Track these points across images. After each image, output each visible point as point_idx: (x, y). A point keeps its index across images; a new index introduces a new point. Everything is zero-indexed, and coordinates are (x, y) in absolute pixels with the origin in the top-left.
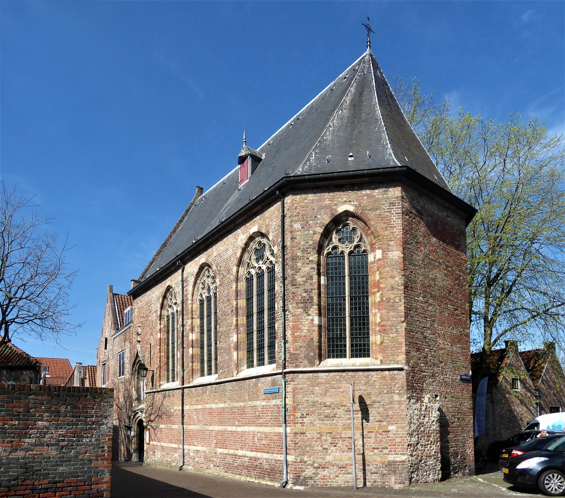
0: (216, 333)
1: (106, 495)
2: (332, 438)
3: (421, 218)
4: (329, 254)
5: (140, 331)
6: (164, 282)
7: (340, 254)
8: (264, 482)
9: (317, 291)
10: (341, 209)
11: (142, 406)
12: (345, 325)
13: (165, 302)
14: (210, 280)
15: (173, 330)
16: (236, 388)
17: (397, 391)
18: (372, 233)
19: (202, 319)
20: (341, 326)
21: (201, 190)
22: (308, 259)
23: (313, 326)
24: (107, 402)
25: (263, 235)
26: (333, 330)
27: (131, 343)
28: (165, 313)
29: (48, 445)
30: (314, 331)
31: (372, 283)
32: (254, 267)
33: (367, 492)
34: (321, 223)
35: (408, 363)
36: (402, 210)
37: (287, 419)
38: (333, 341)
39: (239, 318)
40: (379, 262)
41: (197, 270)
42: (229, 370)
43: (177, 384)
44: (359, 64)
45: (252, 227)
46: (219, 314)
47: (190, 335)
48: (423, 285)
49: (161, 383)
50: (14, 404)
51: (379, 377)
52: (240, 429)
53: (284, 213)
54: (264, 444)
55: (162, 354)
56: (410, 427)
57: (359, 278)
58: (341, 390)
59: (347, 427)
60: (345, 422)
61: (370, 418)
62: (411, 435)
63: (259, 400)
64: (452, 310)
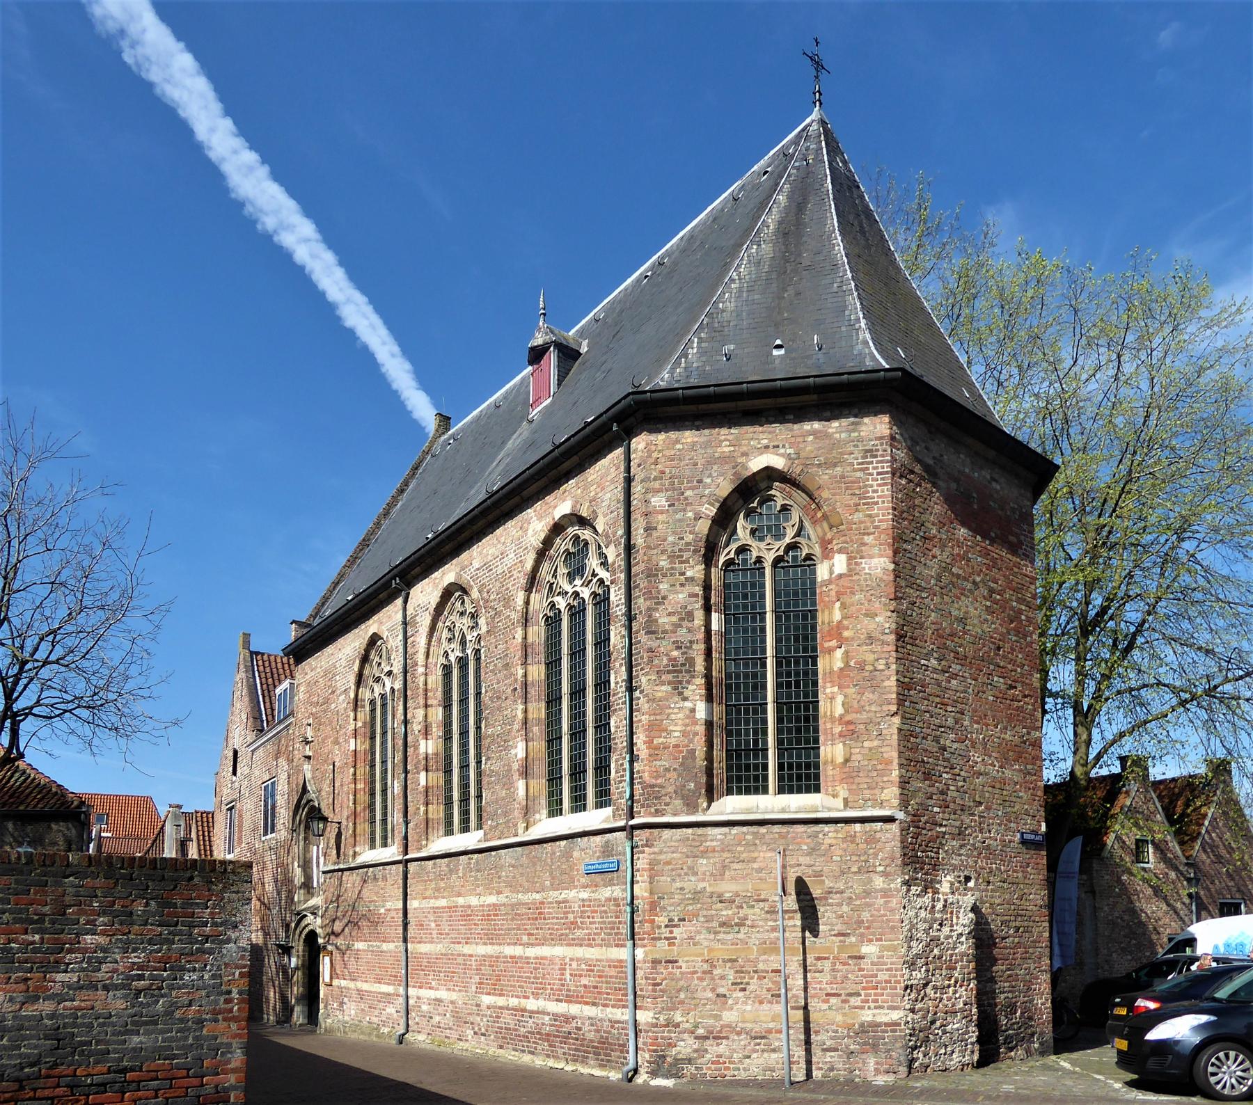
0: (479, 738)
1: (236, 1097)
2: (737, 972)
3: (934, 485)
4: (729, 563)
5: (310, 734)
6: (363, 626)
7: (755, 563)
8: (585, 1070)
9: (702, 646)
10: (757, 464)
11: (315, 901)
12: (765, 721)
13: (367, 669)
14: (466, 621)
15: (384, 733)
16: (524, 860)
18: (825, 517)
19: (447, 707)
20: (756, 723)
22: (683, 574)
23: (695, 723)
24: (238, 892)
25: (583, 522)
26: (739, 733)
27: (290, 761)
28: (365, 694)
29: (106, 988)
30: (696, 734)
31: (826, 628)
32: (563, 593)
33: (813, 1091)
34: (711, 494)
35: (904, 805)
36: (891, 467)
37: (636, 930)
38: (739, 757)
39: (529, 705)
40: (841, 582)
41: (438, 600)
42: (508, 821)
43: (392, 852)
44: (796, 142)
45: (560, 504)
46: (485, 698)
47: (422, 742)
48: (938, 633)
49: (357, 849)
50: (32, 896)
51: (840, 835)
52: (531, 952)
53: (629, 472)
54: (585, 986)
55: (360, 786)
56: (910, 947)
57: (796, 617)
58: (755, 866)
59: (769, 948)
60: (766, 936)
61: (821, 927)
62: (912, 965)
63: (575, 887)
64: (1003, 687)
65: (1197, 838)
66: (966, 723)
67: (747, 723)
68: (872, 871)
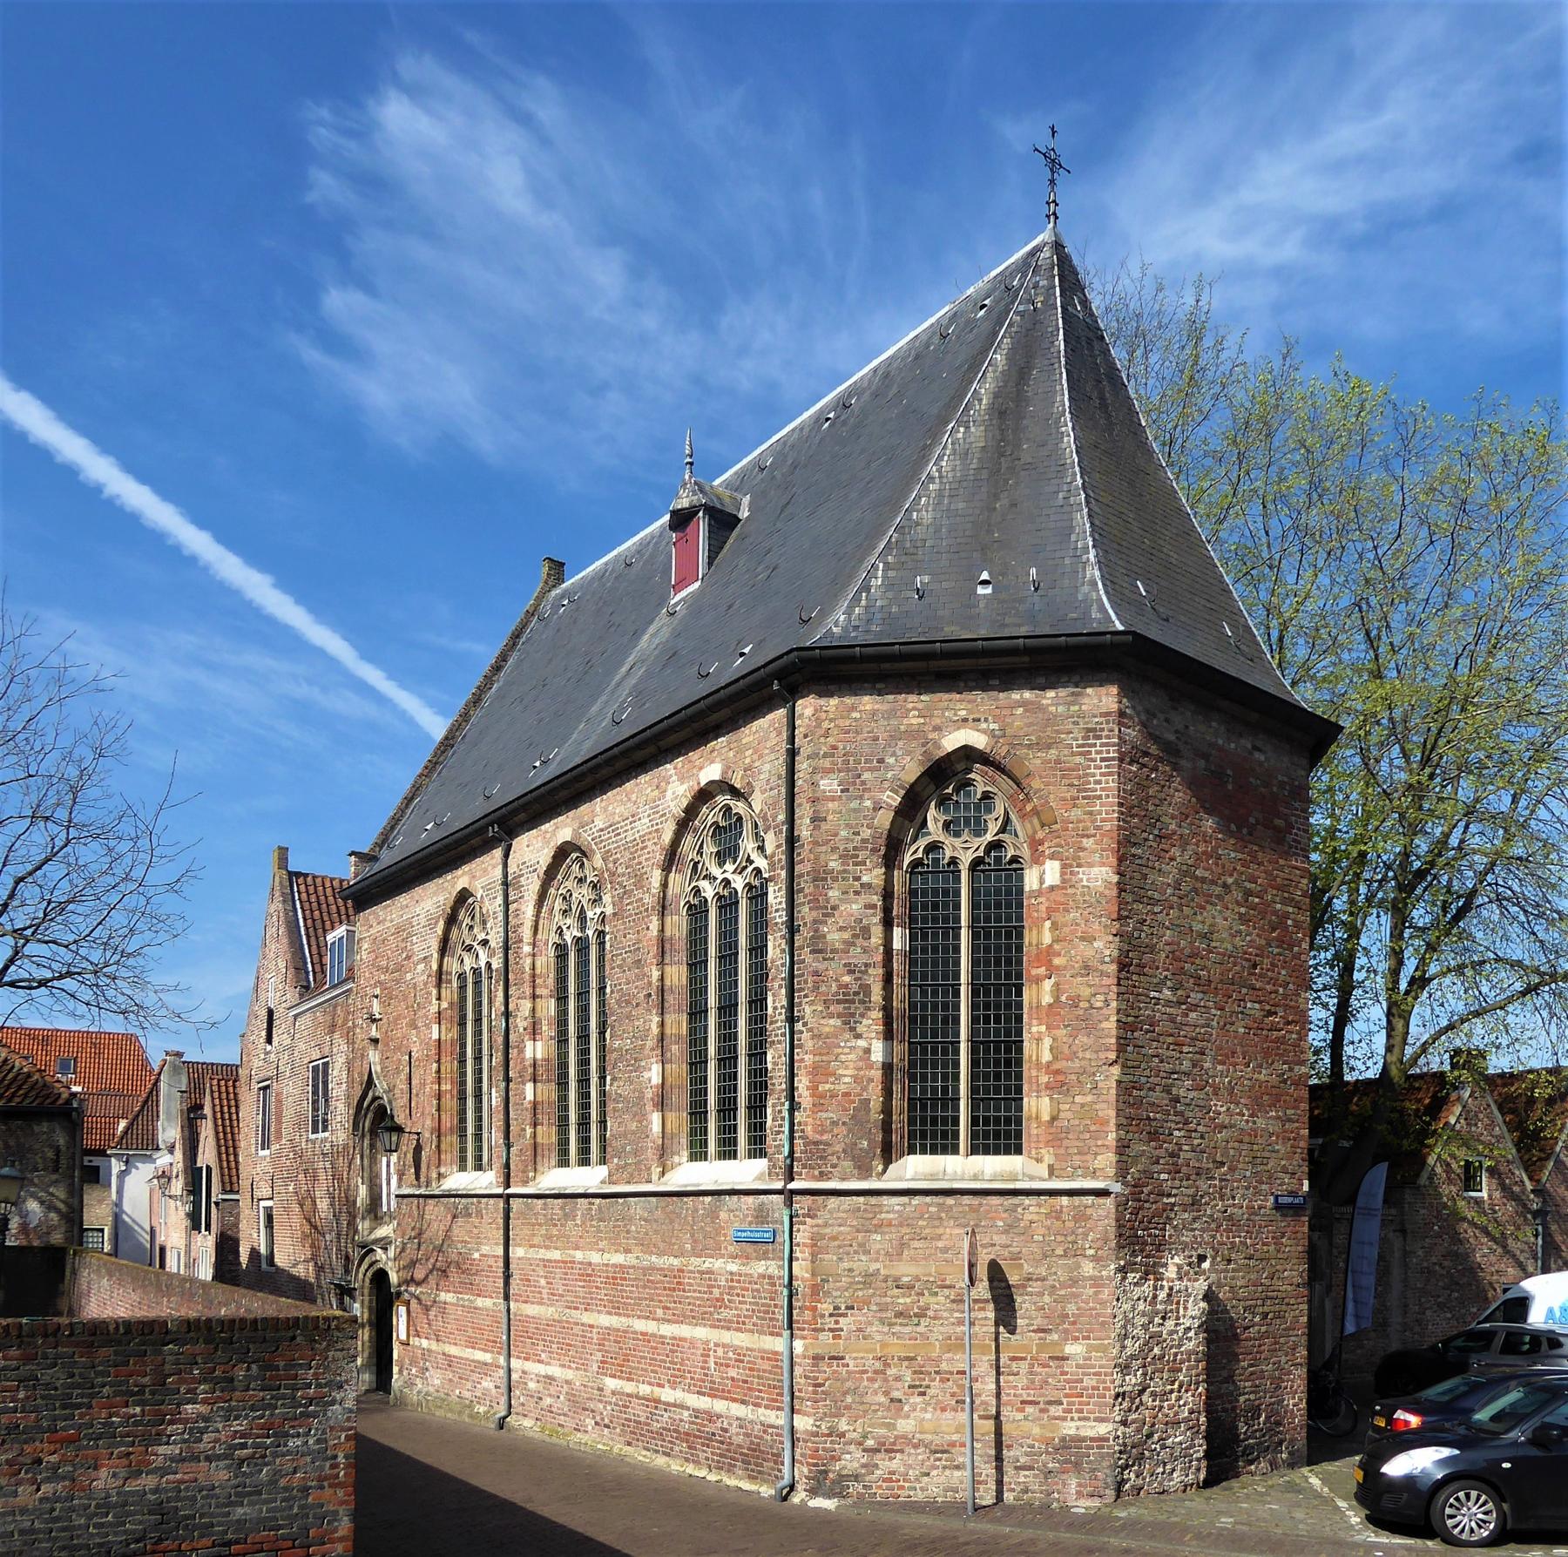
0: (602, 1048)
2: (915, 1372)
4: (916, 863)
5: (376, 1008)
7: (949, 865)
8: (731, 1482)
9: (881, 971)
10: (952, 741)
11: (384, 1231)
12: (957, 1064)
15: (478, 1021)
17: (1092, 1252)
19: (562, 999)
20: (945, 1066)
21: (558, 570)
22: (857, 879)
25: (736, 793)
26: (924, 1078)
27: (351, 1042)
28: (452, 965)
29: (209, 1459)
31: (1034, 951)
33: (998, 1521)
35: (1122, 1174)
36: (1119, 751)
38: (924, 1107)
39: (667, 1017)
40: (1053, 896)
41: (549, 860)
42: (639, 1162)
43: (486, 1181)
45: (707, 765)
46: (612, 1000)
48: (1174, 956)
50: (131, 1367)
52: (668, 1330)
53: (793, 743)
54: (733, 1379)
55: (446, 1087)
57: (998, 935)
58: (940, 1244)
60: (950, 1330)
62: (1125, 1369)
63: (722, 1256)
65: (1547, 1158)
66: (1206, 1065)
67: (934, 1066)
68: (1079, 1254)
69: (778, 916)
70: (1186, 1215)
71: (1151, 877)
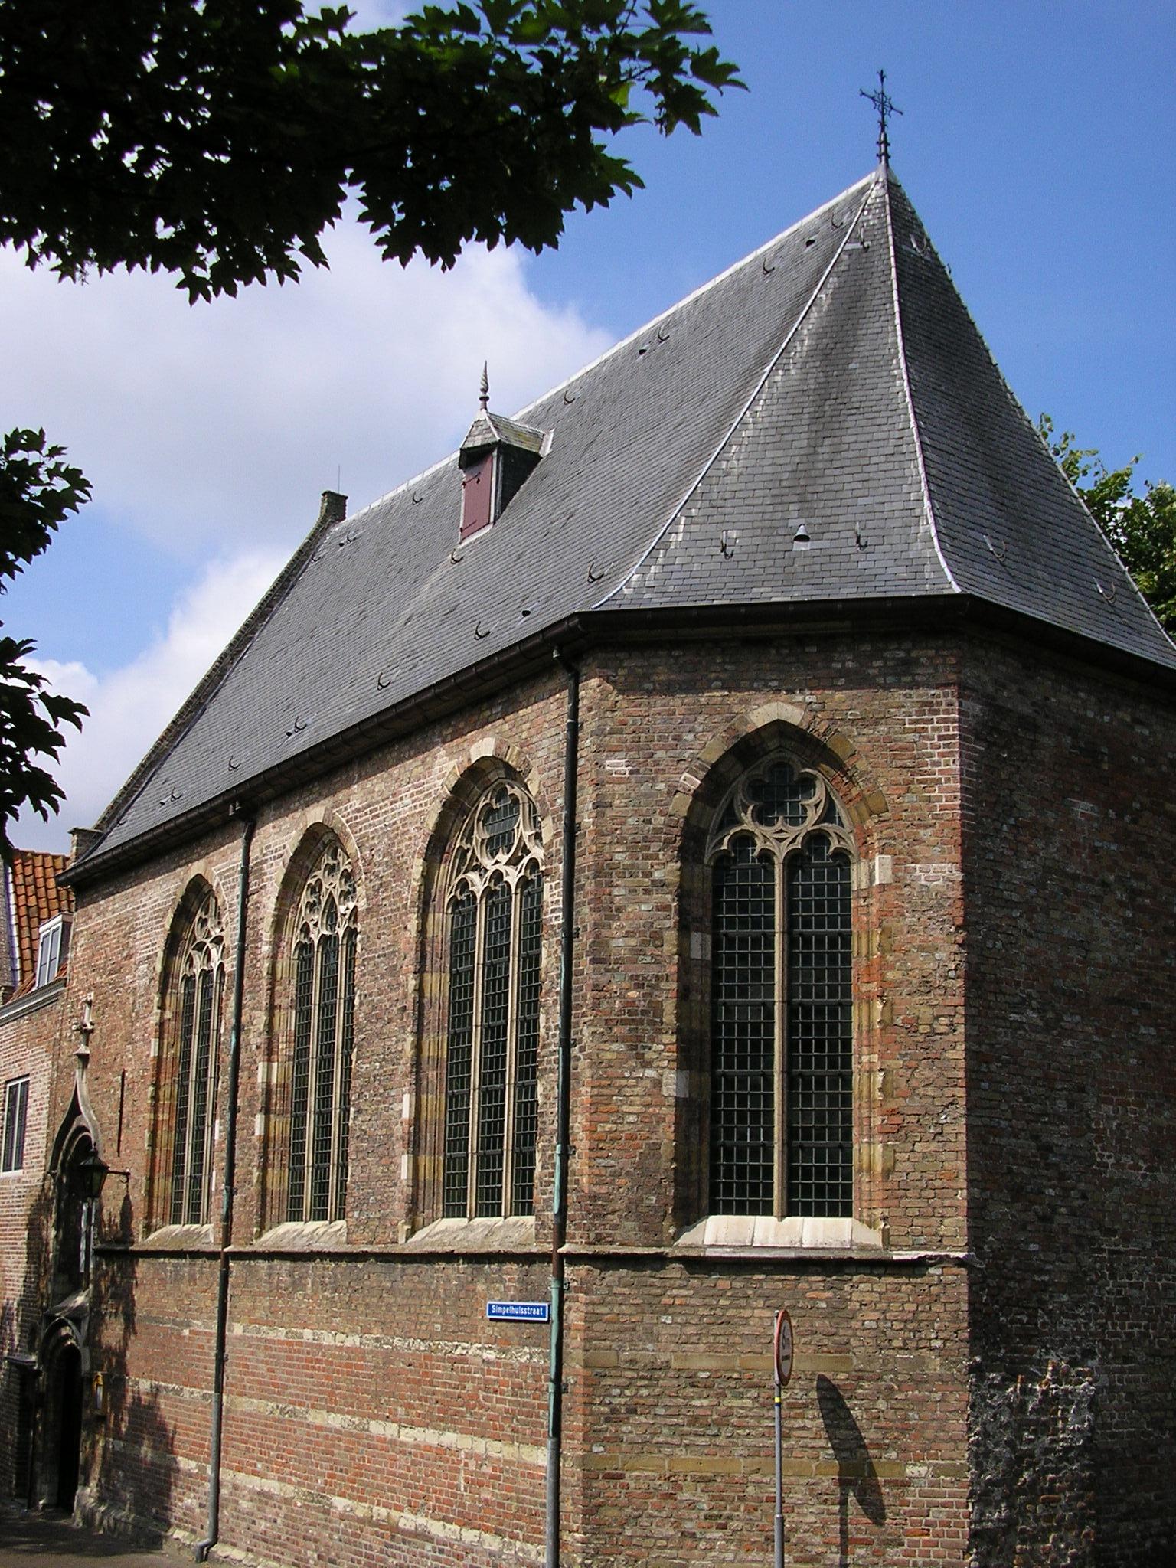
2: (713, 1498)
15: (204, 1038)
17: (938, 1343)
19: (304, 1015)
22: (648, 875)
30: (661, 1120)
32: (479, 869)
34: (693, 757)
35: (975, 1240)
46: (360, 1016)
55: (163, 1116)
69: (553, 917)
70: (1065, 1298)
71: (1007, 874)
